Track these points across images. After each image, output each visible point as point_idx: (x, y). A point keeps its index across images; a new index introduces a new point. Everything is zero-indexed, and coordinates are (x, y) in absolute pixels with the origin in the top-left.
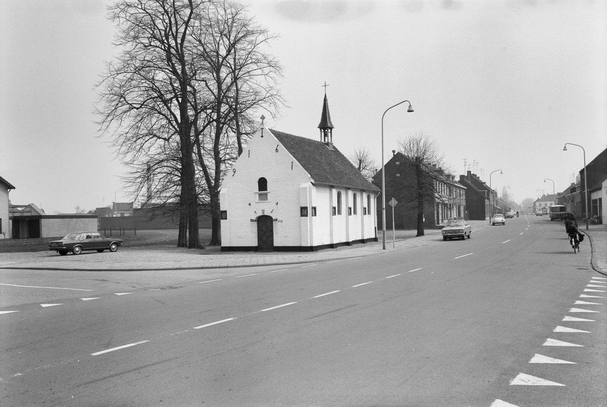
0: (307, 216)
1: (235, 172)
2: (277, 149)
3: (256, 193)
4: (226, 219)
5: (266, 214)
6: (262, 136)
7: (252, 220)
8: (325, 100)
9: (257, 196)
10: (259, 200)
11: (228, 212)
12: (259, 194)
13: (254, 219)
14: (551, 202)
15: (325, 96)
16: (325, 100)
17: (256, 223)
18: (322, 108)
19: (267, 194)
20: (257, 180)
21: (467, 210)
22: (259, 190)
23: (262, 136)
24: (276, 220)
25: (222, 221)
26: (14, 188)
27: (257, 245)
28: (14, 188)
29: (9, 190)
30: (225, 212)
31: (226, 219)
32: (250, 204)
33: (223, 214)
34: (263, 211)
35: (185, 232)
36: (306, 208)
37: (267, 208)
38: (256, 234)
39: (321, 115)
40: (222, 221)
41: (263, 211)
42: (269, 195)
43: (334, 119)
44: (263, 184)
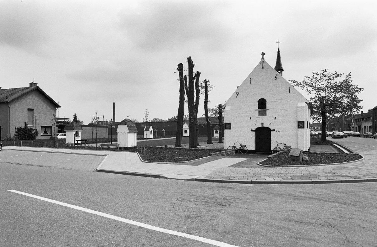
0: (304, 128)
1: (238, 94)
2: (276, 77)
3: (256, 110)
4: (230, 129)
5: (264, 126)
6: (263, 68)
7: (252, 130)
8: (279, 52)
9: (257, 112)
10: (259, 115)
11: (231, 124)
12: (259, 111)
13: (254, 129)
14: (188, 131)
15: (279, 49)
16: (279, 52)
17: (254, 132)
18: (276, 57)
19: (266, 111)
20: (258, 100)
22: (258, 108)
23: (263, 68)
24: (274, 130)
26: (60, 107)
28: (60, 107)
29: (57, 108)
31: (230, 129)
32: (251, 118)
34: (262, 124)
35: (180, 140)
36: (303, 122)
37: (266, 121)
38: (255, 141)
39: (276, 62)
41: (262, 124)
42: (267, 112)
43: (284, 65)
44: (262, 104)
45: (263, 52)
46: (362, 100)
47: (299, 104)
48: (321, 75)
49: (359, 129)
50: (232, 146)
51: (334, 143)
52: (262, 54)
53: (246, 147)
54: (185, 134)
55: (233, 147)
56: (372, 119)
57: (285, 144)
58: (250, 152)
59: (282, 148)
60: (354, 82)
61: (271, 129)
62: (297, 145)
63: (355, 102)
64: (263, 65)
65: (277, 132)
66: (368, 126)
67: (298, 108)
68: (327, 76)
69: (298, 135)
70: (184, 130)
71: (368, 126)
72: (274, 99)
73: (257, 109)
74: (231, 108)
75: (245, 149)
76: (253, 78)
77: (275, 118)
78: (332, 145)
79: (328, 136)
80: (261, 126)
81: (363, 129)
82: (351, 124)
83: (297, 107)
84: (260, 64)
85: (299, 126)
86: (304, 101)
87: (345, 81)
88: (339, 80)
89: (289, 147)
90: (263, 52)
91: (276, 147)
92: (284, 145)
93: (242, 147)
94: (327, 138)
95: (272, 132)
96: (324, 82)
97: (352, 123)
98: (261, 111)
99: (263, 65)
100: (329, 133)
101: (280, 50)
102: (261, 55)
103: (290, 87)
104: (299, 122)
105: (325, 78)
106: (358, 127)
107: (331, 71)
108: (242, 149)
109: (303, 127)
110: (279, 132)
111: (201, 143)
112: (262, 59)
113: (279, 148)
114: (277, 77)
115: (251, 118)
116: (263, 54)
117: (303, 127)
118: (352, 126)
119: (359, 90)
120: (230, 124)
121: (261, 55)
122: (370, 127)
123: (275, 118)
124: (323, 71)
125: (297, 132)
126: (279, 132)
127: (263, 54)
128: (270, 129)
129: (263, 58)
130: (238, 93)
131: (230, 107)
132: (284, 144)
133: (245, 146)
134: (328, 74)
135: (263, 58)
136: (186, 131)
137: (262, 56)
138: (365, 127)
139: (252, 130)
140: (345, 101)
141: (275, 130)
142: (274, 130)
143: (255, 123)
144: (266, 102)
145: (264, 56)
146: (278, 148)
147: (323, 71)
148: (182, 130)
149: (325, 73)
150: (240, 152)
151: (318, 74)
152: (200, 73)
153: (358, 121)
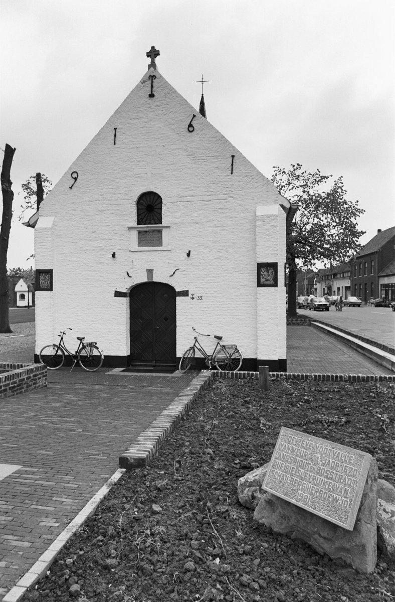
0: (275, 284)
1: (76, 179)
2: (190, 125)
3: (130, 228)
4: (50, 288)
5: (156, 279)
6: (152, 96)
7: (118, 294)
9: (134, 235)
12: (140, 233)
13: (124, 291)
17: (125, 302)
19: (160, 232)
20: (136, 199)
21: (50, 569)
24: (185, 293)
25: (150, 64)
27: (177, 298)
30: (148, 56)
31: (50, 288)
32: (114, 255)
33: (42, 277)
34: (150, 272)
40: (150, 64)
41: (150, 272)
42: (165, 233)
45: (153, 47)
46: (365, 232)
47: (261, 210)
48: (289, 175)
49: (338, 293)
50: (55, 345)
51: (315, 321)
52: (150, 52)
53: (97, 348)
54: (20, 303)
55: (59, 348)
56: (349, 275)
57: (220, 338)
58: (112, 361)
59: (209, 351)
60: (349, 197)
61: (177, 290)
62: (256, 340)
63: (352, 231)
64: (152, 86)
65: (193, 298)
66: (342, 287)
67: (258, 223)
68: (301, 178)
69: (259, 308)
70: (18, 295)
71: (342, 287)
72: (186, 194)
73: (134, 224)
74: (54, 221)
75: (95, 353)
76: (120, 126)
77: (188, 255)
78: (310, 325)
79: (301, 307)
80: (146, 280)
81: (335, 291)
82: (313, 284)
83: (255, 218)
84: (143, 82)
85: (262, 280)
86: (276, 201)
87: (335, 191)
88: (324, 189)
89: (230, 347)
90: (153, 47)
91: (192, 348)
92: (216, 341)
93: (84, 347)
94: (300, 312)
95: (179, 300)
96: (294, 192)
97: (314, 283)
98: (146, 232)
99: (152, 86)
100: (301, 299)
101: (205, 101)
102: (148, 55)
103: (233, 156)
104: (260, 266)
105: (298, 183)
106: (326, 289)
107: (309, 168)
108: (83, 353)
109: (272, 282)
110: (200, 298)
111: (13, 325)
112: (149, 66)
113: (199, 350)
114: (194, 123)
115: (114, 255)
116: (153, 53)
117: (272, 282)
118: (315, 287)
119: (358, 213)
120: (49, 272)
121: (148, 55)
122: (347, 288)
123: (188, 255)
124: (294, 166)
125: (331, 311)
126: (200, 298)
127: (153, 53)
128: (172, 288)
129: (153, 65)
130: (75, 175)
131: (52, 219)
132: (216, 337)
133: (93, 345)
134: (303, 173)
135: (153, 65)
136: (23, 297)
137: (149, 59)
138: (339, 289)
139: (118, 294)
140: (334, 232)
141: (187, 291)
142: (185, 293)
143: (127, 269)
144: (161, 203)
145: (158, 60)
146: (196, 350)
147: (294, 166)
148: (15, 293)
149: (298, 173)
150: (78, 363)
151: (284, 172)
152: (15, 149)
153: (328, 278)
